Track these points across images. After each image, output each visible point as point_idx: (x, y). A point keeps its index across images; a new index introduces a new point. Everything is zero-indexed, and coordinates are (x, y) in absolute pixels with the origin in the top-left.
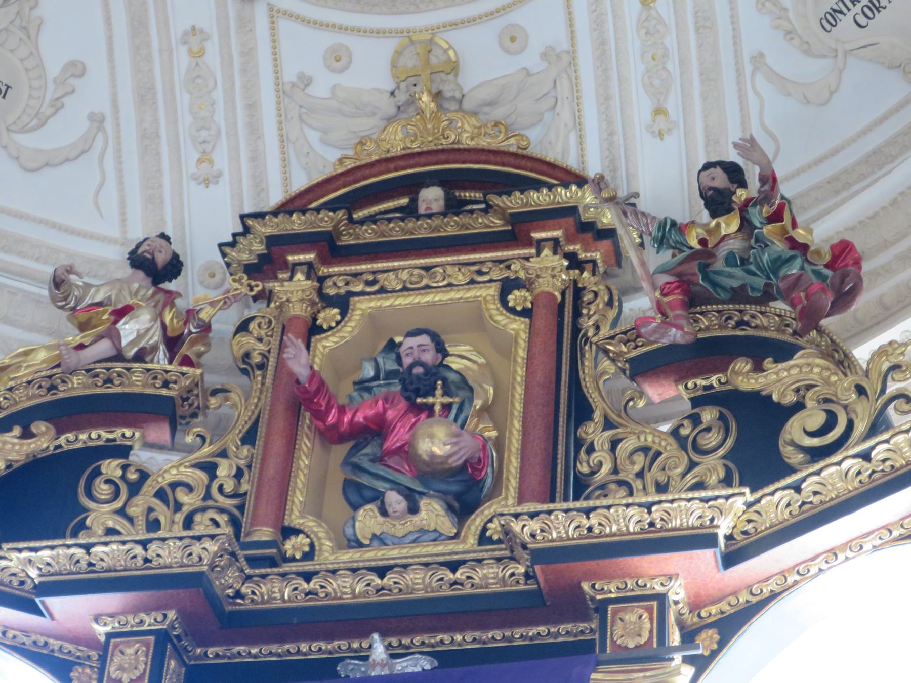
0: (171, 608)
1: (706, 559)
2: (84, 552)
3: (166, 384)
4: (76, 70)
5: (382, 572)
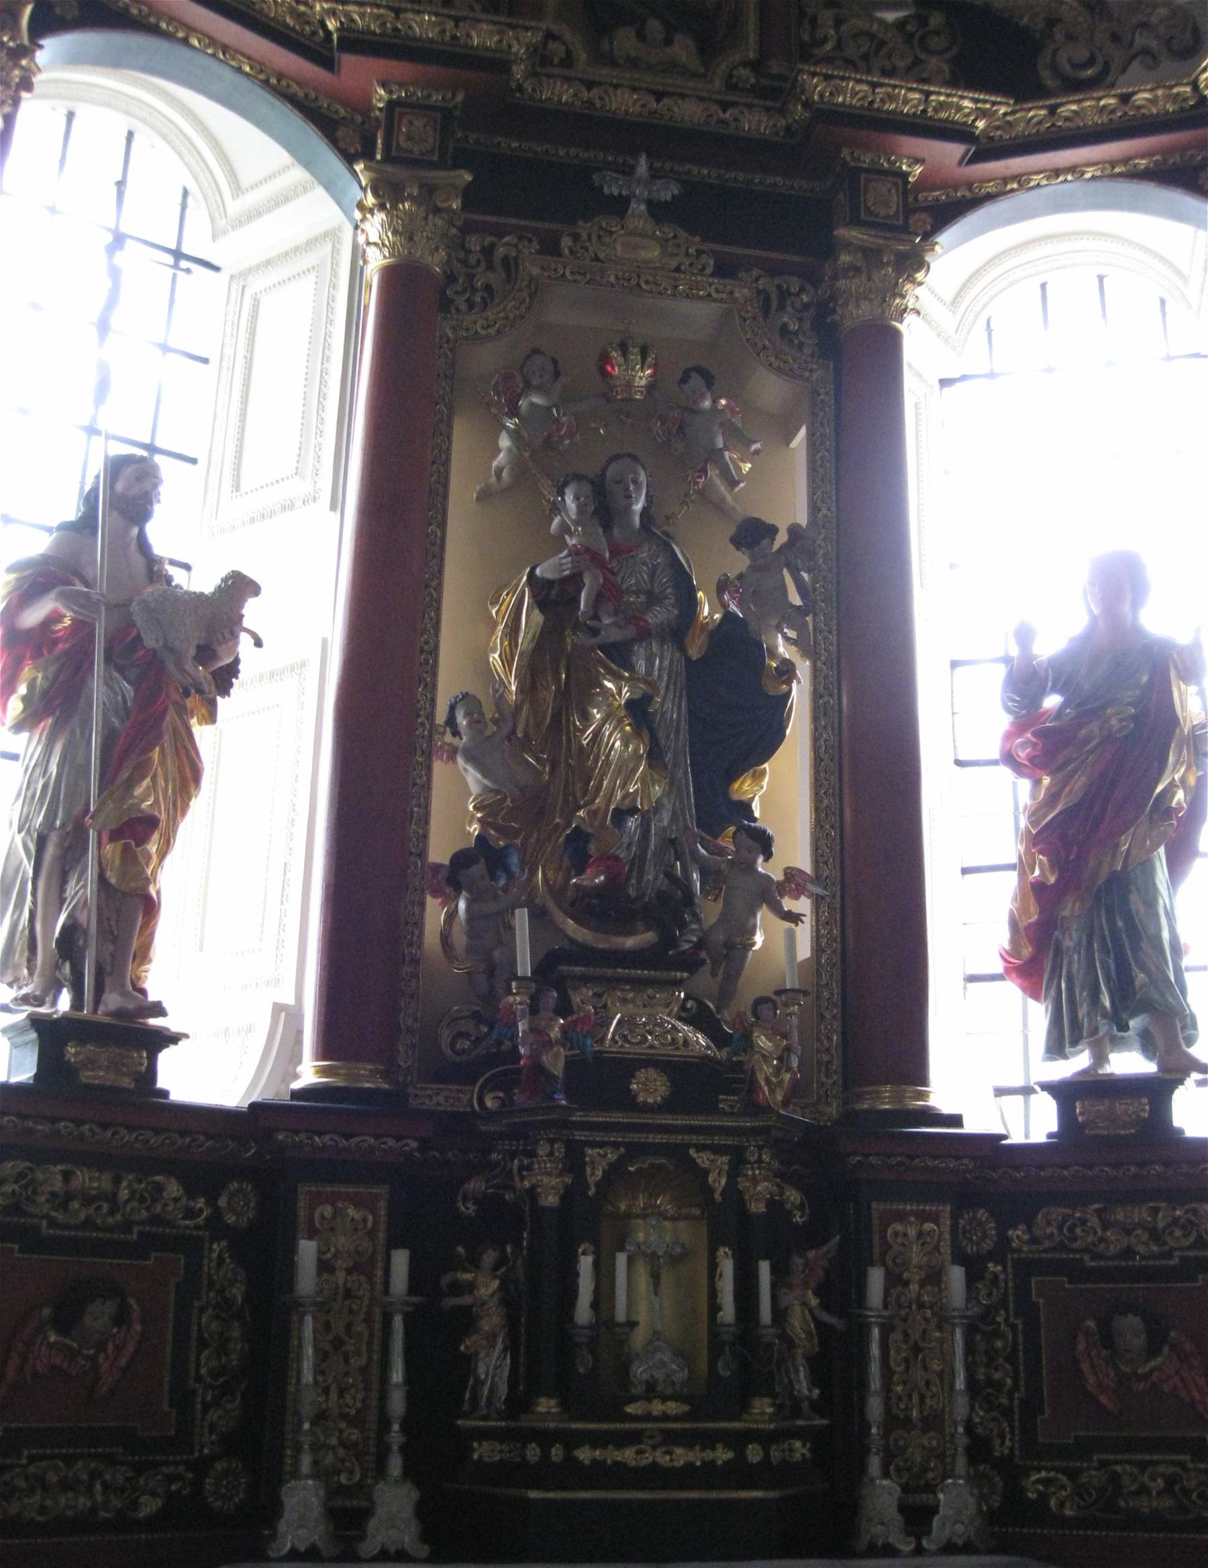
1: (954, 150)
2: (393, 15)
5: (659, 96)
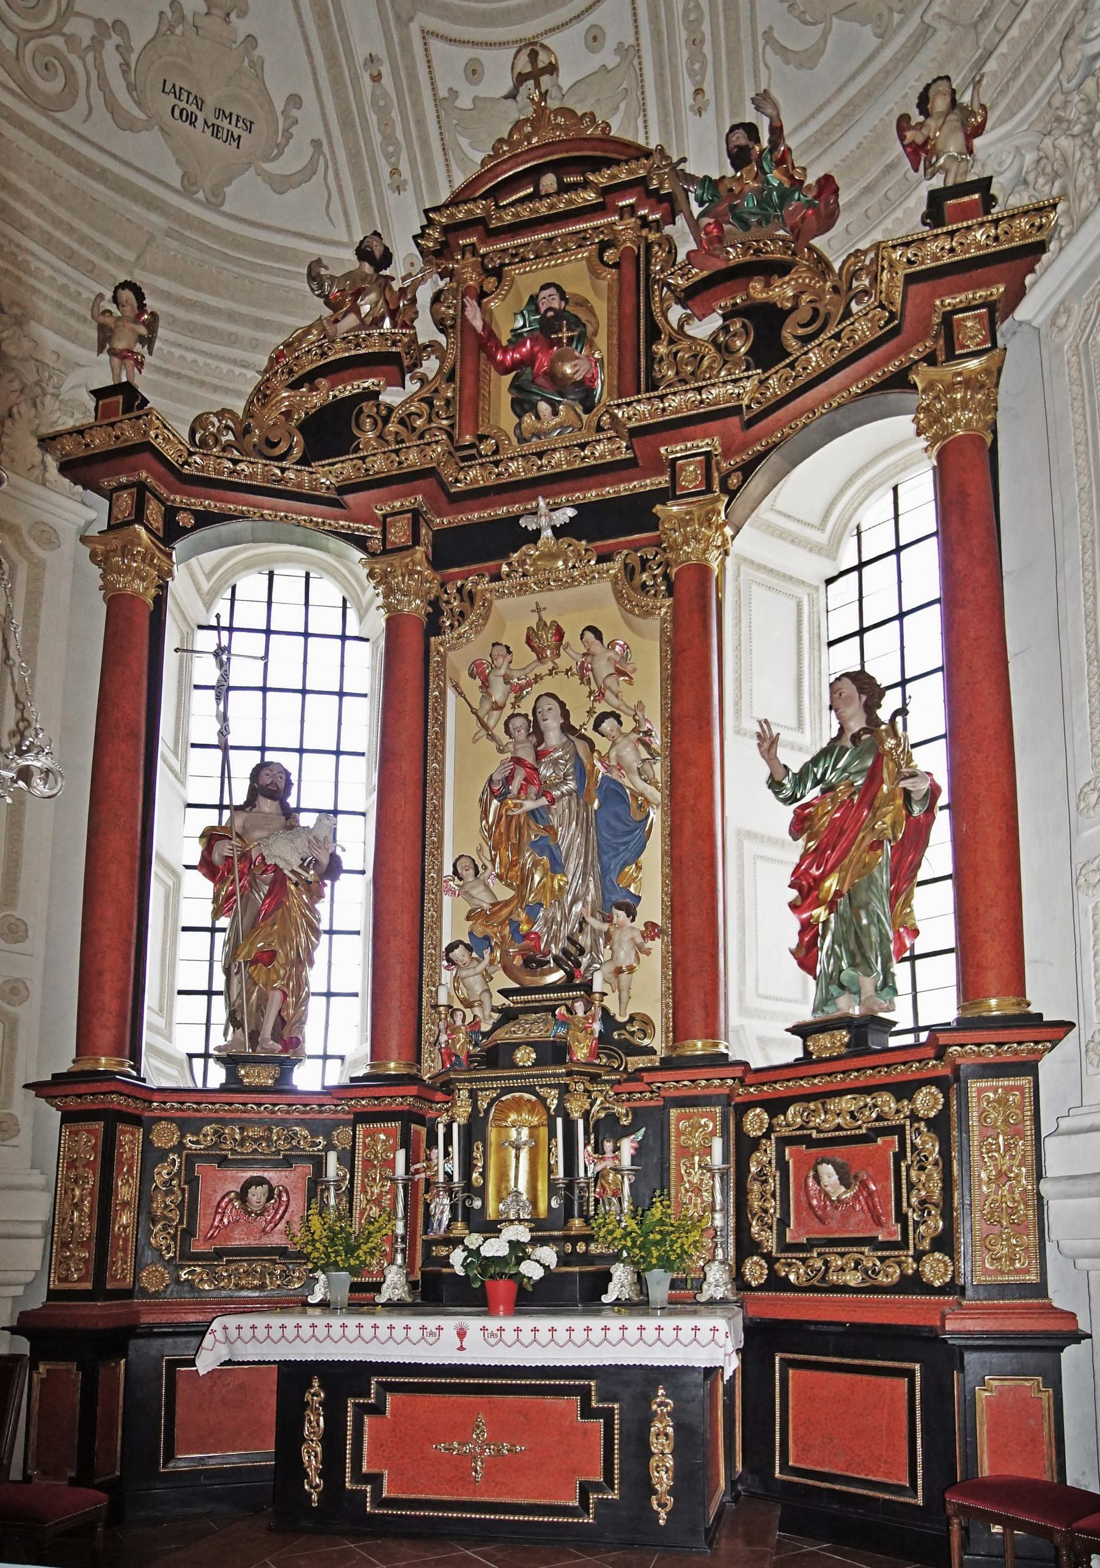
0: (417, 493)
3: (394, 343)
4: (295, 100)
